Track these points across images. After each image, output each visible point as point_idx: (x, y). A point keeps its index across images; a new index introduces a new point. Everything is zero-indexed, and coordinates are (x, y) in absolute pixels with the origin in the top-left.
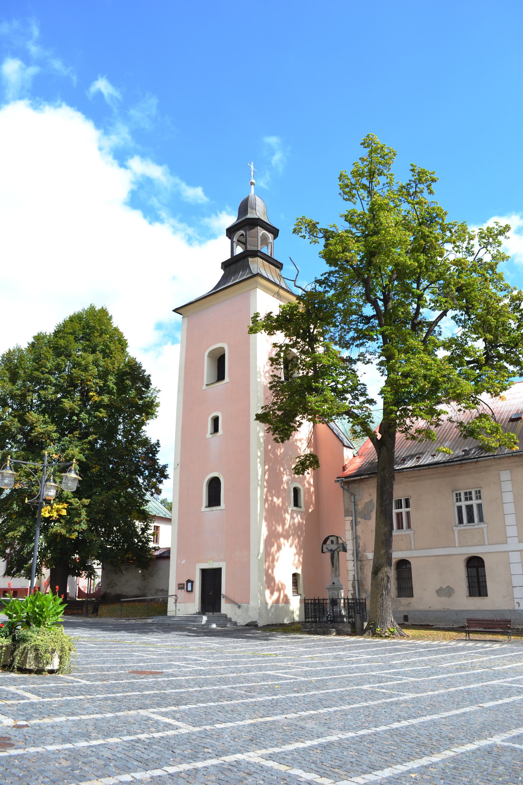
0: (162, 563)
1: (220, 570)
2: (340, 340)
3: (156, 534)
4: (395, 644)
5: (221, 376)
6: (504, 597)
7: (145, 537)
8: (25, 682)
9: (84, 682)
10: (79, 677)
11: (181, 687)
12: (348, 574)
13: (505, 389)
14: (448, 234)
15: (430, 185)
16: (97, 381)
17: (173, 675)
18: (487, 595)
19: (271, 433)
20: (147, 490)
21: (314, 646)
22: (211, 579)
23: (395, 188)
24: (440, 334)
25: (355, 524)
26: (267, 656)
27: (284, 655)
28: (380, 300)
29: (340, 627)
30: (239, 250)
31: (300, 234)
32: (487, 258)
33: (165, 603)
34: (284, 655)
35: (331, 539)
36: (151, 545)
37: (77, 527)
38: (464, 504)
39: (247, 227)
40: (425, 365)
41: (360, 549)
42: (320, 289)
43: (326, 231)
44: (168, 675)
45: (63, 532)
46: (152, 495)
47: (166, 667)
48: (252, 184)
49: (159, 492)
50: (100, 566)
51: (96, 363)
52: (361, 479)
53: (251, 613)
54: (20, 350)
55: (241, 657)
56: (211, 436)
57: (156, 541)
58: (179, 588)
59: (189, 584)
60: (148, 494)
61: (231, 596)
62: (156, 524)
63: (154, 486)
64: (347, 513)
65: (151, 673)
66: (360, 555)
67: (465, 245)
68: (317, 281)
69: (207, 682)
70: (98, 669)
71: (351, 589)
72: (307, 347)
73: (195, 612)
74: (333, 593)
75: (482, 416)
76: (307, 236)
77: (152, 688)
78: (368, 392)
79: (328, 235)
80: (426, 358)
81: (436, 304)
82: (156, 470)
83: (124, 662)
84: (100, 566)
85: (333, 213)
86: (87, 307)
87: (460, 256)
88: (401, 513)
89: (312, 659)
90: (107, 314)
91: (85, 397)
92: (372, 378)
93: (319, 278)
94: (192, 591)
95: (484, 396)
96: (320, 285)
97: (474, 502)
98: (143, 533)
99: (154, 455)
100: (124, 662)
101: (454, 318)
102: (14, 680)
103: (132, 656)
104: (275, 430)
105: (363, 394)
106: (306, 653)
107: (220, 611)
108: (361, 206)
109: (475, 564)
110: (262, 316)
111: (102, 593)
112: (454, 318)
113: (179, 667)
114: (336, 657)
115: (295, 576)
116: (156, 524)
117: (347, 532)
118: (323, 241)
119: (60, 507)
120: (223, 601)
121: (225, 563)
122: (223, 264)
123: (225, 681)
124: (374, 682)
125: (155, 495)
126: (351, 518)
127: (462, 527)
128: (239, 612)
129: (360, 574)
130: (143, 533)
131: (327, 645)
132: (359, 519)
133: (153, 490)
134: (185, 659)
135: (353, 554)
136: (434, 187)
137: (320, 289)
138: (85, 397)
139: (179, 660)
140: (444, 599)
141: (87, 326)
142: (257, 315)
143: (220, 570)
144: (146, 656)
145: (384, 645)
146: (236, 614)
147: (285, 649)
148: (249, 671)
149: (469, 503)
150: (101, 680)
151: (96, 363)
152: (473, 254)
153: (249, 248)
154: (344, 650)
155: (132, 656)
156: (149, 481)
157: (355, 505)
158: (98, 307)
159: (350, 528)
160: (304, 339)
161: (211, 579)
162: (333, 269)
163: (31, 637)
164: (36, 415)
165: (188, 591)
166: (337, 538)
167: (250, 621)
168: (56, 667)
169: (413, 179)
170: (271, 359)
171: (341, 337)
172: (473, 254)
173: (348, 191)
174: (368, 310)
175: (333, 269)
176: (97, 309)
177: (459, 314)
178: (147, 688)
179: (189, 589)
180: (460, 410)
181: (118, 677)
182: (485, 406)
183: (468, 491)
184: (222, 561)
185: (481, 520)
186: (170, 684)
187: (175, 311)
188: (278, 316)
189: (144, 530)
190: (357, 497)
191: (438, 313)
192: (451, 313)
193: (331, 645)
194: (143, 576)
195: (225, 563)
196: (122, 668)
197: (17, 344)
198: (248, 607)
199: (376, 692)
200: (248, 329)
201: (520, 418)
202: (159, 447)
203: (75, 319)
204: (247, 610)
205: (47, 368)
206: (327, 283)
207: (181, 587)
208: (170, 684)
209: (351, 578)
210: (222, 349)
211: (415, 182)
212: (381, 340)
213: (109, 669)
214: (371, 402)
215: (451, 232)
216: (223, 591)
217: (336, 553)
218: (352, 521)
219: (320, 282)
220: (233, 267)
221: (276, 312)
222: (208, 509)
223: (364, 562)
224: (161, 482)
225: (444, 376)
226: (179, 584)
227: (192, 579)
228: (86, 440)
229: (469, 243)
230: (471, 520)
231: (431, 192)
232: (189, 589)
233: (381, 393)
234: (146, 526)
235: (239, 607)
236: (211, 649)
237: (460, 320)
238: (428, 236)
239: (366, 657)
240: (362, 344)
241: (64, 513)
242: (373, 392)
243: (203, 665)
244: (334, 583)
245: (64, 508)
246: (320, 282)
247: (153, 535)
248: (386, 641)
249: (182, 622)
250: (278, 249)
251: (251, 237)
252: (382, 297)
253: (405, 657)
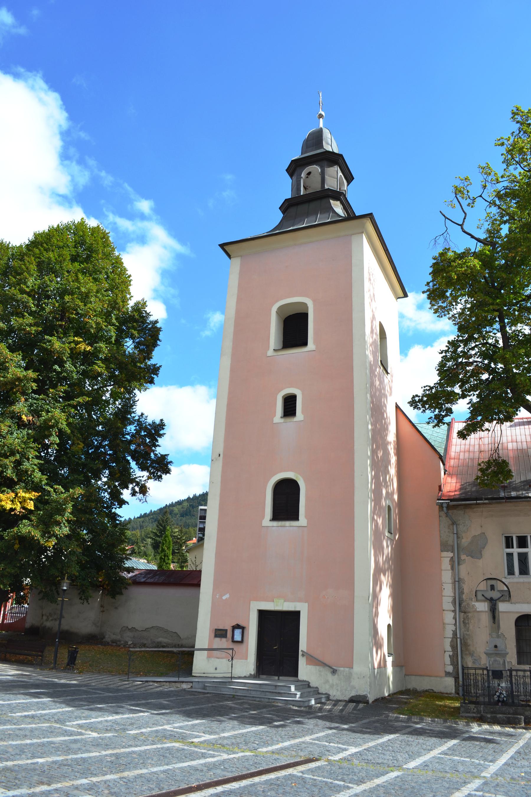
1: (296, 615)
12: (444, 628)
25: (455, 564)
37: (56, 529)
39: (325, 163)
41: (464, 597)
45: (37, 534)
46: (134, 494)
48: (321, 116)
52: (477, 504)
53: (355, 682)
56: (282, 420)
58: (216, 636)
59: (238, 632)
61: (317, 654)
64: (445, 547)
66: (464, 604)
71: (448, 648)
73: (248, 674)
74: (495, 661)
94: (242, 642)
107: (297, 677)
111: (27, 625)
115: (389, 626)
117: (443, 573)
119: (27, 495)
120: (302, 662)
121: (306, 605)
126: (451, 555)
128: (333, 679)
129: (463, 630)
132: (463, 557)
135: (454, 602)
143: (296, 615)
146: (327, 681)
157: (458, 538)
159: (449, 567)
165: (233, 641)
167: (353, 694)
179: (238, 637)
184: (300, 600)
194: (102, 606)
195: (306, 605)
198: (351, 674)
204: (349, 678)
205: (28, 287)
207: (220, 633)
209: (449, 633)
210: (305, 305)
216: (303, 646)
218: (452, 558)
220: (292, 210)
222: (275, 523)
223: (470, 615)
226: (216, 630)
227: (242, 624)
232: (238, 637)
235: (334, 672)
241: (31, 506)
244: (496, 647)
245: (31, 499)
249: (254, 694)
251: (329, 176)
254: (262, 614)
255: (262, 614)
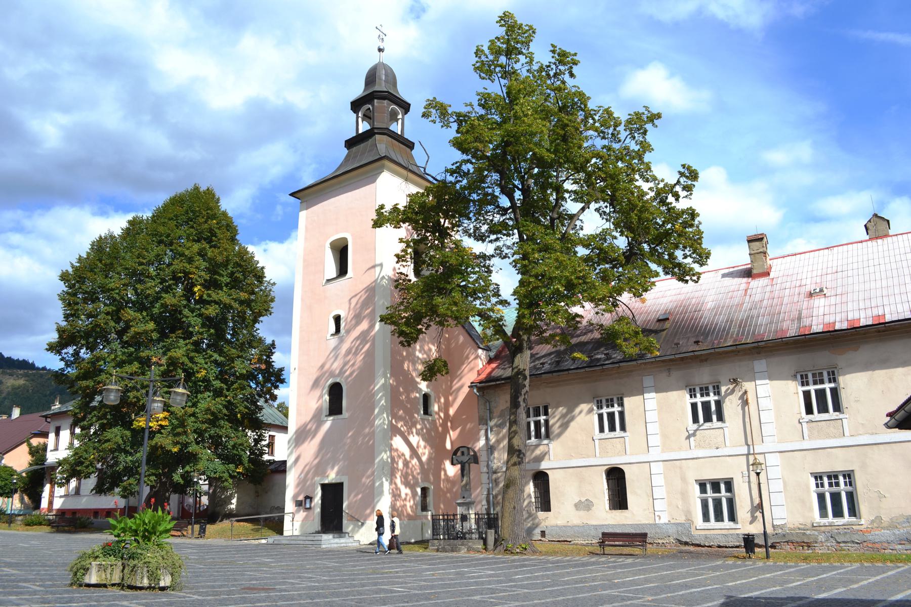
0: (278, 477)
2: (475, 232)
3: (271, 445)
4: (525, 560)
5: (342, 270)
6: (645, 510)
7: (258, 450)
8: (136, 598)
9: (196, 597)
10: (190, 593)
11: (293, 600)
13: (646, 290)
14: (591, 121)
15: (571, 67)
16: (203, 273)
17: (285, 591)
18: (626, 508)
19: (397, 335)
20: (260, 396)
21: (439, 563)
22: (333, 494)
23: (535, 67)
24: (582, 229)
26: (387, 573)
27: (404, 572)
28: (519, 189)
29: (470, 544)
30: (364, 127)
31: (430, 119)
32: (634, 147)
33: (281, 521)
34: (404, 572)
35: (461, 450)
36: (266, 457)
38: (699, 399)
40: (560, 265)
42: (450, 179)
43: (458, 115)
44: (281, 591)
46: (266, 401)
47: (279, 584)
49: (274, 398)
50: (207, 482)
51: (202, 254)
54: (112, 237)
55: (359, 574)
57: (272, 453)
59: (308, 501)
60: (262, 400)
62: (272, 433)
63: (269, 391)
65: (263, 589)
67: (611, 131)
68: (447, 171)
69: (318, 596)
70: (208, 587)
72: (436, 242)
75: (621, 319)
76: (438, 120)
77: (264, 601)
78: (501, 293)
79: (461, 119)
80: (564, 258)
81: (578, 197)
82: (271, 374)
83: (235, 580)
84: (207, 482)
85: (467, 92)
86: (190, 187)
87: (605, 142)
88: (709, 402)
89: (433, 575)
90: (214, 195)
91: (189, 292)
92: (506, 279)
93: (450, 167)
95: (626, 297)
96: (451, 175)
97: (542, 418)
98: (256, 445)
99: (269, 357)
100: (235, 580)
101: (597, 210)
102: (126, 596)
103: (244, 575)
104: (402, 333)
105: (497, 294)
106: (428, 570)
108: (496, 87)
109: (616, 477)
110: (388, 207)
112: (597, 210)
113: (293, 584)
114: (457, 573)
116: (272, 433)
118: (455, 126)
122: (346, 141)
123: (337, 595)
124: (486, 594)
125: (270, 402)
127: (603, 436)
130: (256, 445)
131: (452, 563)
133: (268, 396)
134: (300, 577)
136: (575, 70)
137: (450, 179)
138: (189, 292)
139: (293, 578)
140: (582, 513)
141: (191, 209)
142: (382, 207)
144: (258, 575)
145: (514, 561)
147: (407, 567)
148: (364, 586)
149: (705, 399)
150: (213, 595)
151: (202, 254)
152: (620, 141)
153: (377, 125)
154: (468, 566)
155: (244, 575)
156: (263, 386)
157: (490, 412)
158: (203, 188)
160: (433, 233)
161: (333, 494)
162: (465, 157)
163: (141, 554)
164: (132, 313)
166: (468, 448)
168: (168, 584)
169: (553, 60)
170: (397, 256)
171: (476, 229)
172: (620, 141)
173: (485, 69)
174: (505, 202)
175: (465, 157)
176: (201, 190)
177: (604, 206)
178: (259, 601)
180: (597, 313)
181: (229, 593)
182: (625, 307)
183: (609, 397)
185: (623, 428)
186: (282, 598)
187: (292, 195)
188: (405, 207)
189: (257, 441)
190: (493, 404)
191: (580, 205)
192: (593, 206)
193: (457, 562)
196: (233, 586)
197: (109, 230)
199: (484, 602)
200: (372, 223)
201: (668, 319)
202: (274, 348)
203: (177, 201)
206: (458, 173)
208: (282, 598)
210: (345, 240)
211: (555, 64)
212: (517, 236)
213: (221, 586)
214: (505, 303)
215: (593, 119)
217: (467, 465)
219: (452, 172)
221: (403, 203)
224: (277, 387)
225: (578, 278)
228: (191, 341)
229: (615, 129)
230: (708, 419)
231: (572, 75)
233: (515, 293)
234: (261, 435)
236: (328, 568)
237: (605, 212)
238: (567, 125)
239: (490, 572)
240: (497, 240)
242: (506, 293)
243: (318, 581)
246: (452, 172)
247: (268, 446)
248: (516, 557)
250: (410, 125)
252: (520, 187)
253: (530, 572)
254: (324, 486)
255: (324, 486)
